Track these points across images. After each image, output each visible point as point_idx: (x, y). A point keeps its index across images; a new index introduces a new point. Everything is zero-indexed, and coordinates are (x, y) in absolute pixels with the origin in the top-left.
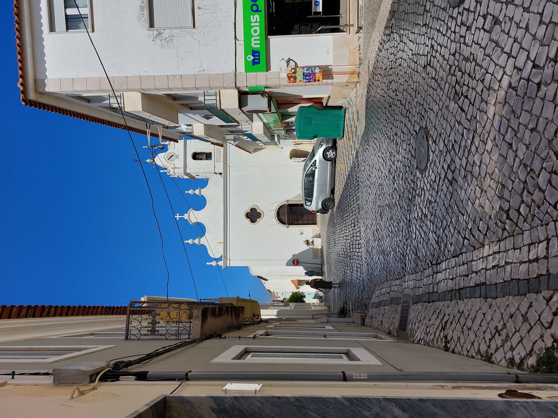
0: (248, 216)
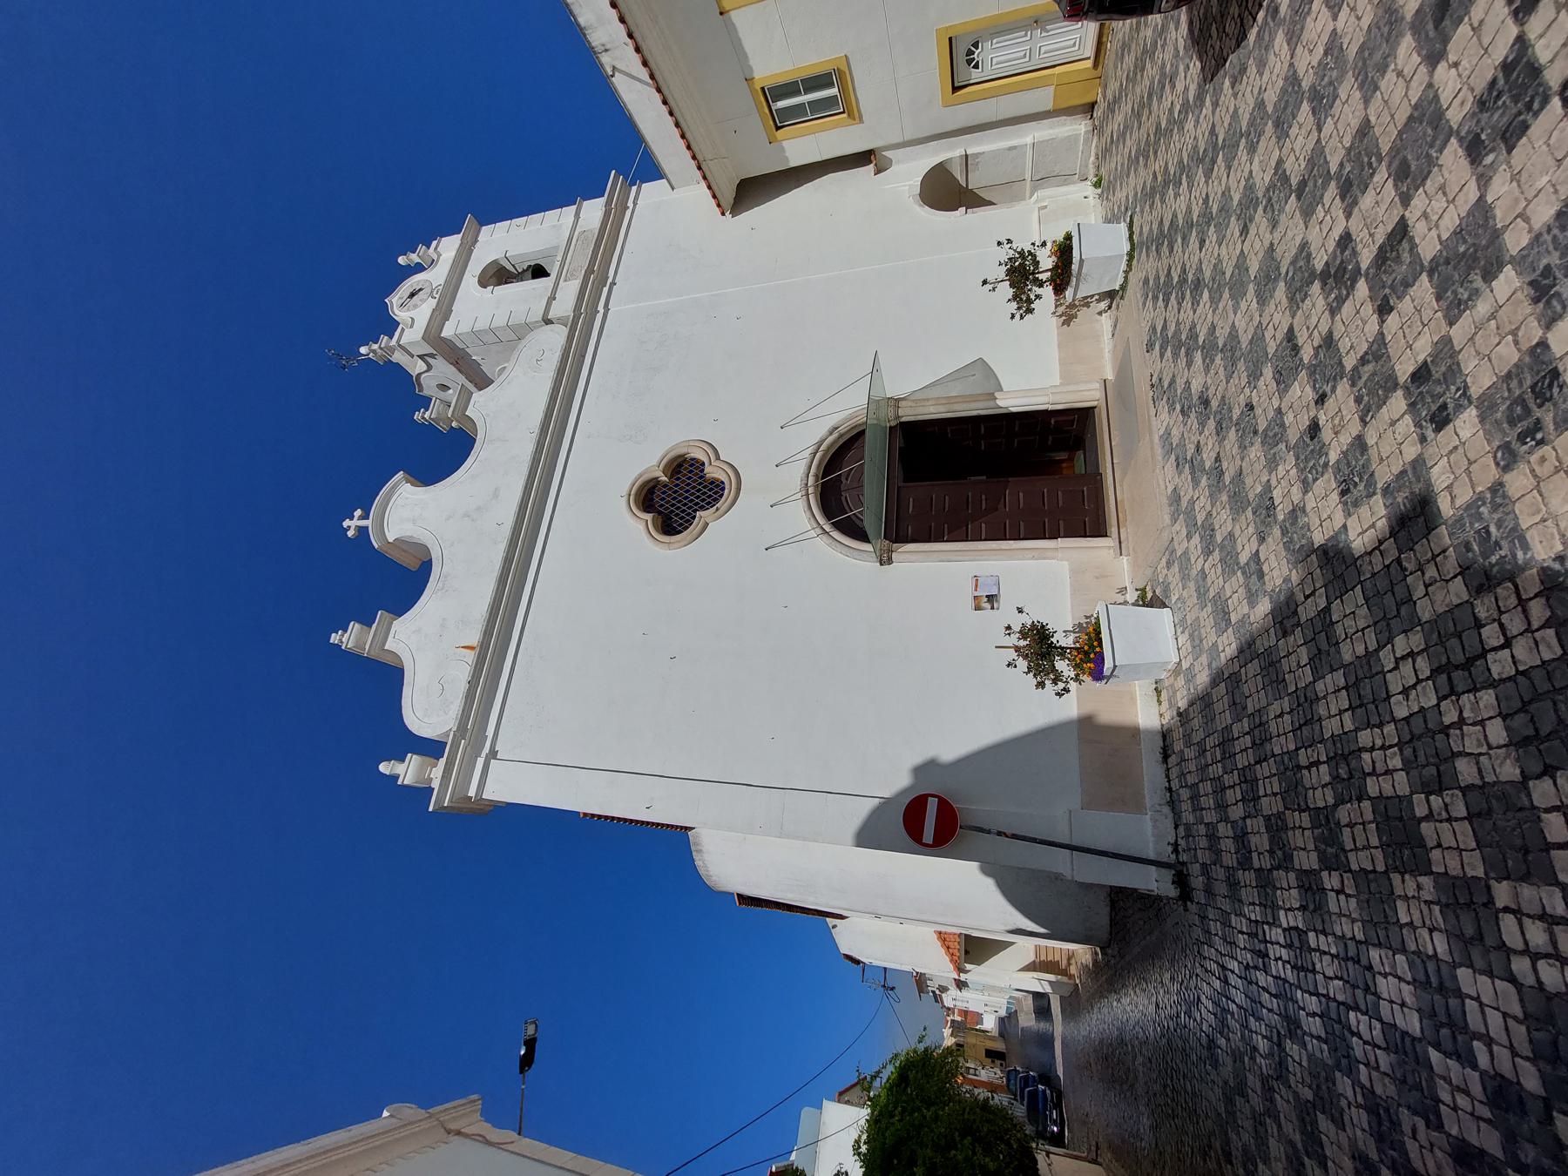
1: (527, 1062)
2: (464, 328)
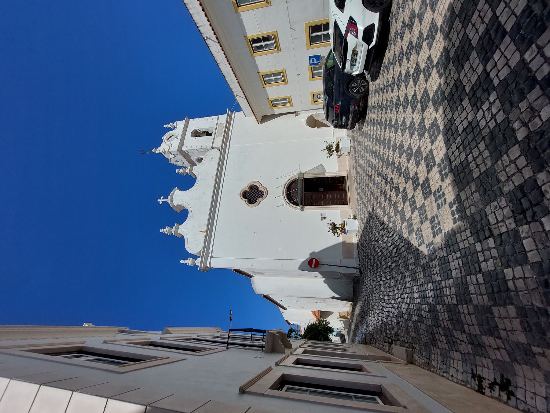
0: (245, 195)
1: (231, 319)
2: (189, 148)
